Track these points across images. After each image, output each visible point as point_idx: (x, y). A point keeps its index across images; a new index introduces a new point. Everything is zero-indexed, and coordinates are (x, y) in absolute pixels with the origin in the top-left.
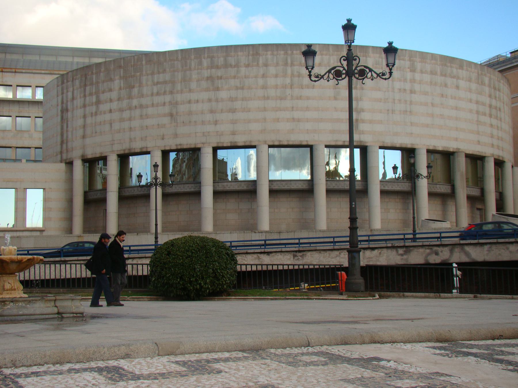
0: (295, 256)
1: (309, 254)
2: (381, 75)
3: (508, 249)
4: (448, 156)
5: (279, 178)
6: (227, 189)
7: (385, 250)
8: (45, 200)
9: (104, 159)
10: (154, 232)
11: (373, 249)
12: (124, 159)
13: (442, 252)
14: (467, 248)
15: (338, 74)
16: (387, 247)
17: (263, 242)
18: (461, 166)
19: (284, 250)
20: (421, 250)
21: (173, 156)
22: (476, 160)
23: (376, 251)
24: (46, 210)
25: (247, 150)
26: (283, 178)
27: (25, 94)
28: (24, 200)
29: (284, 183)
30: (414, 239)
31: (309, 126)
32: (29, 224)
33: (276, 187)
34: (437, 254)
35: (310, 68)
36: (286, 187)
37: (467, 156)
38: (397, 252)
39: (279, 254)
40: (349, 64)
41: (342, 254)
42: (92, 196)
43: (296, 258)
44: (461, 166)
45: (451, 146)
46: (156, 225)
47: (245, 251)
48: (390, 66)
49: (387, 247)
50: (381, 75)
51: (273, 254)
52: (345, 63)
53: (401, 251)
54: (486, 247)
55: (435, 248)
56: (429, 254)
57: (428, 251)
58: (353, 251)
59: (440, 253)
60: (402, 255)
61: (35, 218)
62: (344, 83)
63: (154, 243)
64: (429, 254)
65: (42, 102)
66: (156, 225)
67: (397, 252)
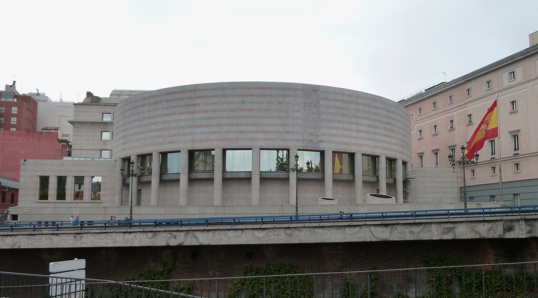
0: (75, 237)
1: (85, 235)
3: (226, 235)
4: (374, 158)
5: (231, 171)
7: (138, 234)
10: (295, 203)
11: (130, 233)
13: (179, 236)
14: (197, 234)
16: (140, 232)
17: (104, 225)
18: (383, 164)
19: (487, 219)
20: (164, 234)
22: (391, 161)
23: (132, 234)
26: (233, 171)
29: (233, 173)
31: (249, 136)
33: (264, 176)
34: (175, 238)
36: (235, 176)
37: (387, 158)
38: (147, 235)
39: (64, 235)
41: (108, 236)
42: (145, 179)
43: (76, 239)
44: (383, 164)
45: (376, 152)
46: (131, 202)
47: (481, 219)
49: (140, 232)
51: (61, 235)
53: (150, 235)
54: (211, 233)
55: (174, 233)
56: (169, 238)
57: (169, 235)
59: (177, 237)
60: (150, 238)
63: (464, 208)
64: (169, 238)
66: (131, 202)
67: (147, 235)
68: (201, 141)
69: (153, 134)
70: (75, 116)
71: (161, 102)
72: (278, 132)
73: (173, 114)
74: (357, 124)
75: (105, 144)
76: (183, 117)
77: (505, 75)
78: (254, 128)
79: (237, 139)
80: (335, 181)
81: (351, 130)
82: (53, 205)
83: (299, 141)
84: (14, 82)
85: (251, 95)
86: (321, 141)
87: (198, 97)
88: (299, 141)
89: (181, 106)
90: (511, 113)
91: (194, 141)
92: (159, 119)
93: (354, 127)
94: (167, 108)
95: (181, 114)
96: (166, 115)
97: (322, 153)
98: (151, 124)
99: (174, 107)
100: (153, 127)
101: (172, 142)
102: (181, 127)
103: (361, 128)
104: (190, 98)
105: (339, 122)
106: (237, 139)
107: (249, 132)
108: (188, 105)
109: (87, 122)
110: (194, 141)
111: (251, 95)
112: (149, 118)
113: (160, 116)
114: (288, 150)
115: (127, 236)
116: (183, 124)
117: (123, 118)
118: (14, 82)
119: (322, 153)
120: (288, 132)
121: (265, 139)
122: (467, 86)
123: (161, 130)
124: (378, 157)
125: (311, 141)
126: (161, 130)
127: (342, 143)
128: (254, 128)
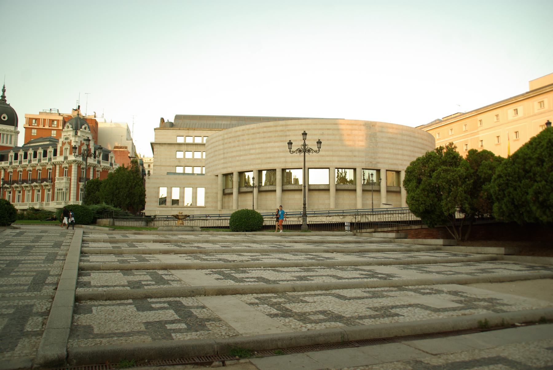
2: (316, 151)
6: (289, 189)
8: (206, 193)
9: (232, 173)
11: (330, 216)
12: (241, 174)
15: (300, 151)
20: (349, 217)
21: (264, 173)
24: (206, 197)
25: (531, 90)
27: (198, 140)
28: (196, 193)
30: (373, 211)
32: (198, 205)
33: (312, 188)
35: (290, 148)
40: (305, 147)
42: (227, 191)
48: (319, 148)
50: (316, 151)
52: (303, 147)
53: (341, 217)
58: (305, 215)
61: (201, 202)
62: (303, 154)
65: (178, 200)
68: (292, 162)
69: (253, 157)
70: (155, 138)
71: (259, 133)
72: (348, 156)
73: (269, 142)
74: (402, 150)
75: (179, 161)
76: (277, 144)
77: (510, 110)
78: (331, 153)
79: (319, 161)
80: (388, 192)
81: (398, 154)
82: (170, 209)
83: (363, 162)
84: (79, 107)
85: (328, 129)
86: (378, 163)
87: (288, 130)
88: (363, 162)
89: (275, 137)
90: (515, 140)
91: (286, 162)
92: (257, 146)
93: (400, 152)
94: (264, 138)
95: (275, 142)
96: (263, 143)
97: (378, 171)
98: (250, 149)
99: (269, 137)
100: (252, 152)
101: (269, 163)
102: (276, 152)
103: (405, 153)
104: (282, 131)
105: (390, 148)
106: (319, 161)
107: (327, 156)
108: (281, 136)
109: (165, 144)
110: (286, 162)
111: (328, 129)
112: (248, 145)
113: (258, 143)
114: (355, 170)
115: (328, 218)
116: (277, 149)
117: (223, 144)
118: (79, 107)
119: (378, 171)
120: (355, 156)
121: (339, 161)
122: (479, 117)
123: (259, 154)
124: (400, 171)
125: (371, 162)
126: (259, 154)
127: (392, 164)
128: (331, 153)
